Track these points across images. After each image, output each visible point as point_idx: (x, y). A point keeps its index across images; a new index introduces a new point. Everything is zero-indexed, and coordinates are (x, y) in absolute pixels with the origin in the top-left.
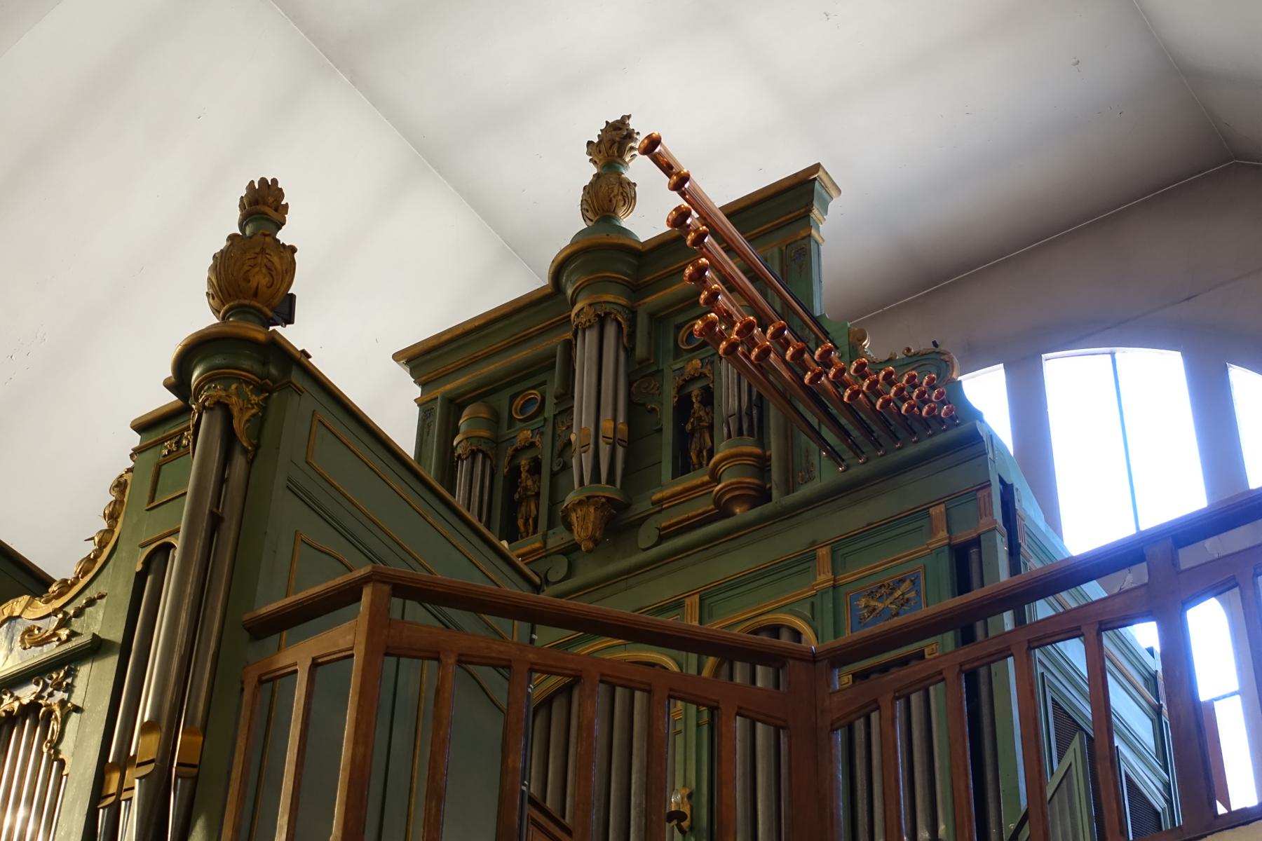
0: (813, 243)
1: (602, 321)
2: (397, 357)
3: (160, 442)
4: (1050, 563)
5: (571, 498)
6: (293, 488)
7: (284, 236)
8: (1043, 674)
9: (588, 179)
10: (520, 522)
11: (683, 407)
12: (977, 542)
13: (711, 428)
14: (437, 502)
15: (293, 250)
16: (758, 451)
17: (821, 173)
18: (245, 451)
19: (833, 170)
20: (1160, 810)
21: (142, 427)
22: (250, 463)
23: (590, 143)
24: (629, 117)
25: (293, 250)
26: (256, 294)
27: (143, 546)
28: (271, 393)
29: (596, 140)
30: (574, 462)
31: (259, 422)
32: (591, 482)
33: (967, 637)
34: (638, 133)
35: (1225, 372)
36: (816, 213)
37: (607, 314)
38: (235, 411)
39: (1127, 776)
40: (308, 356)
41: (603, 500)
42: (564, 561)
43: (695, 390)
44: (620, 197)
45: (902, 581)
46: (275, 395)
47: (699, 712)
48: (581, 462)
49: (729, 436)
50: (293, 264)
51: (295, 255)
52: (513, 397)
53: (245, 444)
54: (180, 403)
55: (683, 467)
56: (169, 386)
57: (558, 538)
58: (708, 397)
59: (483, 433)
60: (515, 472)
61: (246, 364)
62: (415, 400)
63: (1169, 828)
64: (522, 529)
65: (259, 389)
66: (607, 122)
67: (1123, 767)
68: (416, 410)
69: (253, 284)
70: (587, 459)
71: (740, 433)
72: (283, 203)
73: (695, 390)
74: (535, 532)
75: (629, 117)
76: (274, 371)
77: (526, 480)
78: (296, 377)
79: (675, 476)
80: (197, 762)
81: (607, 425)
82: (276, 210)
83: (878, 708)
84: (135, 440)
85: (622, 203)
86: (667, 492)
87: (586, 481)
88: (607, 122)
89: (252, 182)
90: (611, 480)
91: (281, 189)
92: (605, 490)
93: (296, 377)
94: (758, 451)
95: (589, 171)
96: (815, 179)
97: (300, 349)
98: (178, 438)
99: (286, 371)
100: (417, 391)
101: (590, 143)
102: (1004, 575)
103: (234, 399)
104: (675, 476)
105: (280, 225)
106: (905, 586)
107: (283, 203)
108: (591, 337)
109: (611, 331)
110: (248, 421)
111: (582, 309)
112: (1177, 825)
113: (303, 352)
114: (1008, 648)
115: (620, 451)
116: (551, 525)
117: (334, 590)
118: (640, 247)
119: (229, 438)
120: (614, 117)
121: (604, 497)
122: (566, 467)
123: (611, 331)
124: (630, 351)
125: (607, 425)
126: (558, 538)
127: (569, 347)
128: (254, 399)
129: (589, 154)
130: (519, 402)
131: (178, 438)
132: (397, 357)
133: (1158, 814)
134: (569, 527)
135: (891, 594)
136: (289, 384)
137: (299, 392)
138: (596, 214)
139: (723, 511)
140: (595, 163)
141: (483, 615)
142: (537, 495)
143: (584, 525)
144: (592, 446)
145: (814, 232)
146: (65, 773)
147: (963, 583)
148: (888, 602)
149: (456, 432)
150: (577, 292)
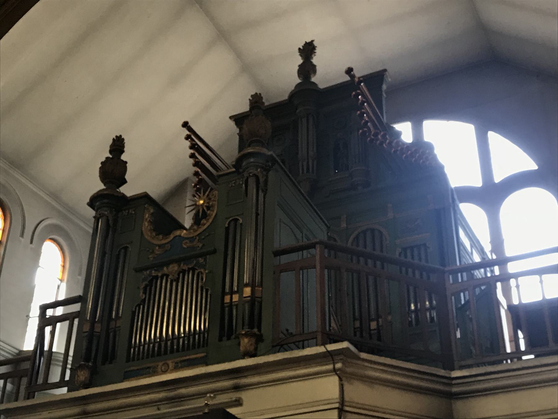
2: (231, 118)
4: (471, 262)
14: (260, 266)
15: (126, 163)
23: (299, 49)
25: (126, 163)
29: (301, 48)
32: (307, 173)
47: (352, 275)
63: (451, 277)
66: (306, 42)
70: (305, 163)
87: (305, 172)
88: (306, 42)
90: (313, 172)
101: (299, 49)
102: (458, 264)
108: (304, 120)
115: (315, 163)
117: (194, 385)
120: (308, 40)
125: (311, 153)
132: (231, 118)
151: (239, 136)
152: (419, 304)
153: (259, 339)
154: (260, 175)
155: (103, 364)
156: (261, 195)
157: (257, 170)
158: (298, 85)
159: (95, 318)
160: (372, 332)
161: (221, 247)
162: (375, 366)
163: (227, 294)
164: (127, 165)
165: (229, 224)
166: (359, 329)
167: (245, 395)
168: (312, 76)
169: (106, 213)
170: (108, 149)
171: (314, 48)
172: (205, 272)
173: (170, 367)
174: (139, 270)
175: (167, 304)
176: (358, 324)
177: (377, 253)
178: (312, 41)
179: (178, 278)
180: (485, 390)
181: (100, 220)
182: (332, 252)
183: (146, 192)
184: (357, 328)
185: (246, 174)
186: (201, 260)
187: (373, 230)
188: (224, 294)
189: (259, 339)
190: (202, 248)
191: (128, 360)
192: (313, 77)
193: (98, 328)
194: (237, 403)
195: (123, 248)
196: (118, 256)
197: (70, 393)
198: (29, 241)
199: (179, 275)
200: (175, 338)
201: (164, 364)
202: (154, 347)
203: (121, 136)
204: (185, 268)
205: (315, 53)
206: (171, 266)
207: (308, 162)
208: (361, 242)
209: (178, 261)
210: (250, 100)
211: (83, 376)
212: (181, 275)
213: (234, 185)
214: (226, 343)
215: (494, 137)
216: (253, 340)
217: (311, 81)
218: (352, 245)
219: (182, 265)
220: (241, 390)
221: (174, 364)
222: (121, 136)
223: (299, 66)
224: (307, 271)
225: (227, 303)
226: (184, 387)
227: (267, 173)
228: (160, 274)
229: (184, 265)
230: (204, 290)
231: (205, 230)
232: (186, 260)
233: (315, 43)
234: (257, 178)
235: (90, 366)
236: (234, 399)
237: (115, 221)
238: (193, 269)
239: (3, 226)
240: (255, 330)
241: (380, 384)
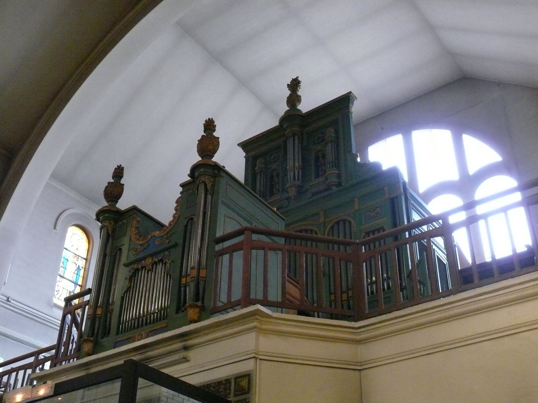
0: (350, 113)
1: (294, 135)
2: (239, 145)
3: (188, 190)
5: (287, 185)
6: (223, 203)
7: (215, 134)
8: (414, 232)
9: (288, 95)
10: (274, 190)
11: (317, 159)
12: (396, 197)
13: (325, 165)
15: (218, 138)
16: (337, 172)
17: (351, 94)
18: (210, 194)
19: (355, 93)
20: (446, 263)
21: (182, 185)
22: (212, 197)
23: (288, 85)
24: (298, 77)
25: (218, 138)
26: (210, 151)
27: (186, 218)
28: (216, 177)
30: (288, 174)
31: (213, 186)
33: (396, 239)
34: (301, 81)
35: (462, 135)
36: (351, 104)
37: (296, 133)
38: (207, 184)
39: (437, 257)
40: (224, 167)
41: (297, 185)
42: (287, 201)
43: (320, 154)
44: (297, 100)
45: (377, 208)
46: (217, 178)
48: (290, 175)
49: (330, 167)
50: (219, 142)
51: (219, 139)
52: (271, 156)
53: (211, 192)
54: (192, 180)
55: (317, 176)
56: (189, 176)
57: (285, 195)
58: (324, 156)
59: (263, 166)
60: (272, 177)
61: (209, 170)
62: (244, 157)
64: (275, 192)
65: (213, 177)
66: (292, 79)
67: (436, 253)
68: (244, 159)
69: (209, 148)
70: (292, 173)
71: (333, 167)
72: (215, 124)
73: (320, 154)
74: (278, 193)
75: (298, 77)
76: (216, 172)
77: (276, 179)
78: (223, 174)
79: (315, 178)
80: (205, 276)
81: (297, 164)
82: (213, 127)
83: (375, 257)
84: (181, 189)
85: (297, 102)
86: (313, 183)
87: (292, 180)
88: (292, 79)
89: (207, 120)
90: (298, 180)
91: (214, 121)
92: (298, 183)
93: (223, 174)
94: (337, 172)
95: (288, 93)
96: (350, 96)
97: (222, 165)
98: (192, 189)
99: (219, 172)
100: (244, 154)
101: (288, 85)
102: (406, 223)
103: (207, 180)
104: (315, 178)
105: (214, 131)
106: (378, 209)
107: (215, 124)
108: (291, 139)
109: (296, 138)
110: (211, 186)
111: (288, 132)
112: (449, 289)
113: (223, 166)
114: (407, 242)
115: (300, 171)
116: (282, 192)
118: (303, 115)
119: (206, 190)
120: (294, 77)
121: (297, 185)
122: (286, 175)
123: (296, 138)
124: (302, 143)
125: (297, 164)
126: (285, 195)
127: (285, 142)
128: (212, 180)
129: (288, 87)
130: (272, 157)
131: (192, 189)
132: (239, 145)
133: (445, 265)
134: (288, 193)
135: (374, 211)
136: (221, 176)
137: (223, 177)
138: (291, 105)
139: (328, 188)
140: (289, 90)
141: (273, 237)
142: (278, 183)
143: (292, 192)
144: (293, 170)
145: (350, 110)
146: (171, 278)
147: (395, 225)
148: (373, 213)
149: (256, 166)
150: (287, 127)
151: (245, 158)
152: (339, 272)
153: (202, 309)
154: (207, 181)
155: (102, 338)
156: (209, 197)
157: (205, 178)
158: (287, 112)
159: (98, 304)
160: (343, 302)
161: (181, 242)
162: (369, 331)
163: (184, 277)
164: (124, 186)
165: (187, 223)
166: (346, 302)
167: (191, 354)
168: (297, 104)
169: (106, 224)
170: (111, 175)
171: (299, 82)
172: (169, 262)
173: (143, 335)
174: (126, 265)
175: (144, 288)
176: (333, 297)
177: (348, 240)
178: (297, 77)
179: (153, 268)
180: (375, 337)
181: (102, 230)
182: (314, 243)
183: (134, 206)
184: (332, 300)
185: (197, 182)
186: (167, 253)
187: (344, 221)
188: (181, 277)
189: (202, 309)
190: (168, 243)
191: (118, 333)
192: (299, 104)
193: (99, 311)
194: (184, 360)
195: (118, 250)
196: (115, 256)
197: (77, 361)
198: (53, 226)
199: (152, 266)
200: (149, 314)
201: (139, 335)
202: (135, 322)
203: (121, 165)
204: (157, 260)
205: (300, 86)
206: (147, 259)
207: (294, 172)
208: (335, 232)
209: (152, 256)
210: (204, 124)
211: (87, 347)
212: (154, 265)
213: (191, 192)
214: (181, 314)
215: (468, 140)
216: (197, 310)
217: (297, 108)
218: (328, 235)
219: (154, 258)
220: (190, 350)
221: (146, 334)
222: (121, 165)
223: (287, 97)
224: (265, 256)
225: (184, 284)
226: (150, 351)
227: (215, 180)
228: (140, 267)
229: (155, 258)
230: (169, 275)
231: (526, 267)
232: (156, 254)
233: (299, 79)
234: (206, 185)
235: (91, 340)
236: (182, 356)
237: (114, 230)
238: (161, 260)
239: (477, 288)
240: (199, 303)
241: (273, 334)
